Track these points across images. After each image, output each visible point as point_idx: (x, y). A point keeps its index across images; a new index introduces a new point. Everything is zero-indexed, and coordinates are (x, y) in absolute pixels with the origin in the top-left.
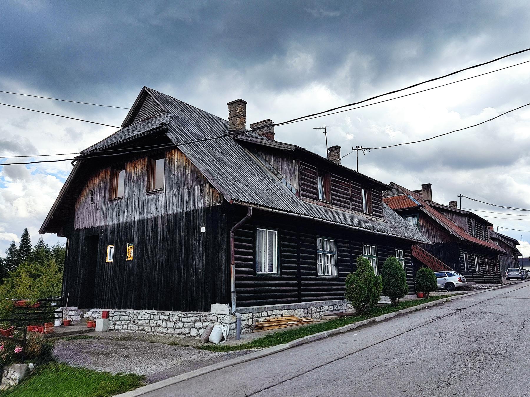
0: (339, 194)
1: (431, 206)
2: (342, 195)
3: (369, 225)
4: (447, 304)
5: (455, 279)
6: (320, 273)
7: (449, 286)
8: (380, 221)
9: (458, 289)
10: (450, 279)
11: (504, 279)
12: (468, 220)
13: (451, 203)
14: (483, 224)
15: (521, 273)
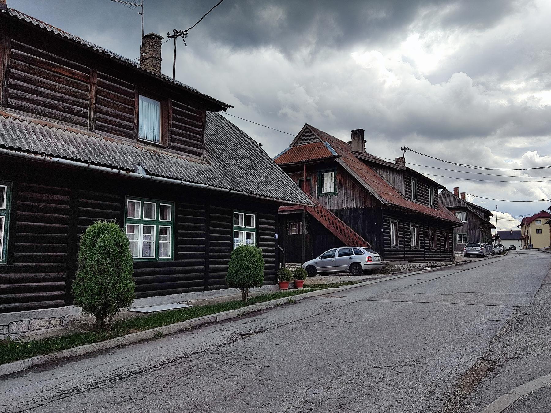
0: (42, 90)
2: (110, 110)
3: (175, 170)
4: (305, 303)
5: (365, 257)
7: (355, 269)
8: (126, 145)
10: (356, 258)
11: (459, 256)
12: (405, 178)
15: (481, 249)
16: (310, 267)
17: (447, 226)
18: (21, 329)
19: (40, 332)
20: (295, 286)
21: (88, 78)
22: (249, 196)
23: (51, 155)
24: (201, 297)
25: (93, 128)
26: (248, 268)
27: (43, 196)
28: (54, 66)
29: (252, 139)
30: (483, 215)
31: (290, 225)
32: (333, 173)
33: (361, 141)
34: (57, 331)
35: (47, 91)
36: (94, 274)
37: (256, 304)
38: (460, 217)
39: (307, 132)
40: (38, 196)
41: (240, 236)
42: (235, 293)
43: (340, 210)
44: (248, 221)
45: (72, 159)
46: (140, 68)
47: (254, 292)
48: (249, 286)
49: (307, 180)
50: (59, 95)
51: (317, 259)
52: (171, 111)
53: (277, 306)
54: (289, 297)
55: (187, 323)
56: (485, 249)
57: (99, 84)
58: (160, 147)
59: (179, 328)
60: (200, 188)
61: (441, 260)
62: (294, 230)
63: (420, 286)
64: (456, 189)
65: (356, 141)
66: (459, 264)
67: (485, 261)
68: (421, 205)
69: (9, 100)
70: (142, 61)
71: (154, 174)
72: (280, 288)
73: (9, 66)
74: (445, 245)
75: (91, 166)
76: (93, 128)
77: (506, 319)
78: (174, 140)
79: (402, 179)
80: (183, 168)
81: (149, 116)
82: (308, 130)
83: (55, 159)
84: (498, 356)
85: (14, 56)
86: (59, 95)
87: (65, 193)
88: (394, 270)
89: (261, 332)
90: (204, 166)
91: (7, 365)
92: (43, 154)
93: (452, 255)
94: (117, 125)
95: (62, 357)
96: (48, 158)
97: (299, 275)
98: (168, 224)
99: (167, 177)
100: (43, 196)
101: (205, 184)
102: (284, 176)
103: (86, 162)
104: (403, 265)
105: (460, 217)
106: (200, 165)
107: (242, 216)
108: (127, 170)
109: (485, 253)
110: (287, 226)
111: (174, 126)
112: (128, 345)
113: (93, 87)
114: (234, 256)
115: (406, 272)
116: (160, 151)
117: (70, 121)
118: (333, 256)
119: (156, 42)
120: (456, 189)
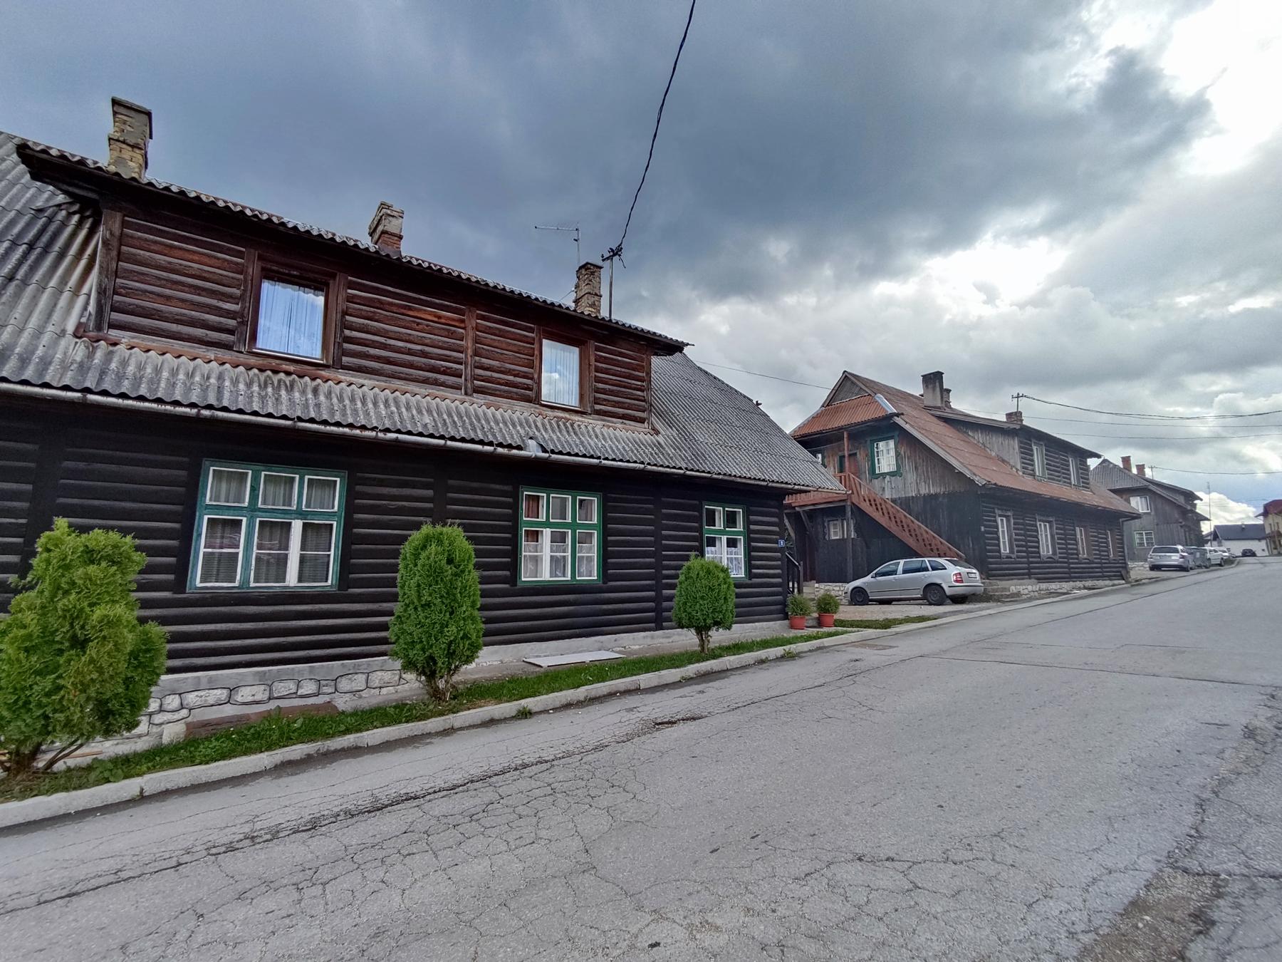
1: (939, 417)
3: (592, 445)
5: (951, 574)
6: (526, 577)
7: (933, 594)
8: (521, 411)
9: (959, 599)
10: (932, 576)
11: (1138, 569)
12: (1021, 442)
13: (1009, 415)
14: (1064, 453)
16: (858, 591)
17: (1111, 520)
18: (355, 686)
19: (384, 691)
20: (820, 623)
21: (463, 321)
23: (387, 430)
24: (649, 641)
25: (469, 391)
26: (702, 598)
27: (394, 491)
30: (1181, 500)
32: (892, 443)
33: (938, 389)
34: (411, 689)
36: (416, 609)
38: (1138, 504)
40: (385, 490)
41: (717, 543)
42: (686, 639)
43: (908, 499)
44: (731, 520)
45: (614, 460)
46: (377, 252)
47: (718, 637)
48: (709, 628)
50: (419, 347)
51: (868, 578)
52: (592, 358)
53: (762, 662)
54: (787, 648)
56: (1190, 558)
57: (477, 328)
58: (576, 412)
59: (564, 701)
60: (634, 470)
61: (1103, 577)
63: (1050, 626)
64: (1126, 460)
65: (930, 390)
66: (1138, 583)
67: (1191, 577)
68: (1055, 485)
69: (345, 359)
70: (576, 301)
71: (553, 452)
72: (792, 627)
73: (345, 313)
74: (1108, 551)
75: (449, 443)
76: (469, 391)
77: (1244, 721)
78: (597, 401)
79: (1015, 443)
80: (613, 441)
81: (560, 371)
82: (847, 380)
83: (393, 436)
84: (1224, 861)
85: (351, 299)
86: (419, 347)
87: (426, 486)
88: (1008, 596)
89: (694, 719)
91: (244, 758)
92: (374, 429)
93: (1125, 567)
95: (339, 747)
96: (381, 435)
98: (738, 533)
99: (577, 455)
100: (394, 491)
102: (803, 453)
103: (442, 437)
104: (1027, 587)
105: (1138, 504)
107: (720, 512)
108: (510, 446)
109: (1191, 564)
111: (598, 380)
112: (461, 729)
114: (682, 578)
115: (1030, 599)
116: (576, 418)
117: (436, 383)
118: (894, 572)
119: (592, 273)
120: (1126, 460)
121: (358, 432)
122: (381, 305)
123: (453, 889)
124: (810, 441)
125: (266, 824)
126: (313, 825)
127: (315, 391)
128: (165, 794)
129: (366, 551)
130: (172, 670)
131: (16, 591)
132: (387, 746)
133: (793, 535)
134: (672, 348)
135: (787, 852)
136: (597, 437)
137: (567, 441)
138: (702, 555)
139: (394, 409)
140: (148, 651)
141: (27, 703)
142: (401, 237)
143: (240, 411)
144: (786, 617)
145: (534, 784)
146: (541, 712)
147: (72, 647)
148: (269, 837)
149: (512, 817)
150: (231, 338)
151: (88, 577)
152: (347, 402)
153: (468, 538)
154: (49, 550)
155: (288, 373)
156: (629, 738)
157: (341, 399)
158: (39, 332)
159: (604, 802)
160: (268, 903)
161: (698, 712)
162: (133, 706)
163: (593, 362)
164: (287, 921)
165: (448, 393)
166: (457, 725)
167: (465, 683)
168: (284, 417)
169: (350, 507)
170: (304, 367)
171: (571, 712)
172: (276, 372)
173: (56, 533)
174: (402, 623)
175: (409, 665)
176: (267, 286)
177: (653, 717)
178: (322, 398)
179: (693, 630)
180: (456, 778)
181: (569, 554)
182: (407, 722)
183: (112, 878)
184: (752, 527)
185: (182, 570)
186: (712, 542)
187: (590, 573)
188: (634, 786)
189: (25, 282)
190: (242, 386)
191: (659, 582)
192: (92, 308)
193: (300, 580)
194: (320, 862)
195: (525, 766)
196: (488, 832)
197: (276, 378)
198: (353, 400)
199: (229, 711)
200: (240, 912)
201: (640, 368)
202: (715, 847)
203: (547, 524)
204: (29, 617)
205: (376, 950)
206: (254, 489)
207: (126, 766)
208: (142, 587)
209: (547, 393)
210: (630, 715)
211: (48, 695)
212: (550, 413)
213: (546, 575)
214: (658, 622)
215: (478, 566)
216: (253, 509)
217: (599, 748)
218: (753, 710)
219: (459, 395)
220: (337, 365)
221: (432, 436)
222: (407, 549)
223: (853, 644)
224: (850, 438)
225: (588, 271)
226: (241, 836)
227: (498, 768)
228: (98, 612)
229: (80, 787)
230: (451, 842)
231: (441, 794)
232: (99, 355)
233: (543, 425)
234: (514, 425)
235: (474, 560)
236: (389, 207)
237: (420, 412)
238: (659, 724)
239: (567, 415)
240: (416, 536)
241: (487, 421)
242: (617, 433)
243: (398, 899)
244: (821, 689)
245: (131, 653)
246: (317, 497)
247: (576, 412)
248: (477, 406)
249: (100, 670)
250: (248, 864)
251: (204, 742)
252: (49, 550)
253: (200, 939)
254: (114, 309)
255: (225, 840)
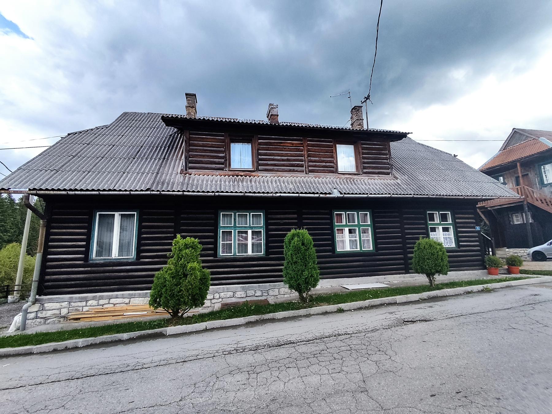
6: (339, 249)
8: (330, 178)
16: (535, 253)
19: (286, 296)
20: (509, 272)
21: (302, 144)
22: (435, 198)
23: (277, 193)
24: (402, 279)
25: (307, 172)
26: (428, 259)
27: (282, 216)
28: (281, 143)
29: (447, 153)
31: (512, 216)
35: (279, 158)
37: (442, 290)
39: (517, 136)
40: (279, 216)
42: (421, 279)
44: (444, 218)
47: (439, 278)
48: (434, 274)
49: (523, 176)
50: (286, 158)
51: (545, 246)
52: (360, 149)
53: (469, 293)
54: (485, 286)
55: (367, 303)
58: (355, 174)
62: (518, 221)
70: (352, 125)
71: (345, 193)
72: (490, 273)
73: (258, 150)
75: (300, 195)
78: (365, 168)
80: (375, 186)
86: (286, 158)
89: (426, 321)
90: (392, 181)
91: (236, 319)
94: (322, 167)
96: (274, 195)
97: (512, 261)
98: (368, 225)
99: (356, 194)
101: (390, 194)
103: (297, 193)
106: (389, 181)
110: (509, 217)
111: (364, 158)
112: (314, 315)
113: (306, 148)
114: (416, 249)
117: (294, 171)
119: (358, 110)
121: (266, 194)
122: (270, 144)
123: (304, 387)
124: (492, 172)
125: (241, 345)
126: (256, 349)
127: (251, 181)
128: (213, 329)
129: (274, 242)
130: (212, 285)
131: (169, 258)
132: (285, 319)
133: (487, 222)
134: (400, 136)
135: (479, 406)
136: (366, 184)
137: (351, 188)
138: (428, 236)
139: (279, 184)
140: (205, 279)
141: (174, 295)
142: (278, 115)
143: (227, 192)
144: (485, 268)
145: (342, 344)
146: (348, 311)
147: (183, 277)
148: (242, 351)
149: (331, 358)
150: (223, 166)
151: (186, 253)
152: (262, 184)
153: (310, 234)
154: (176, 245)
155: (242, 176)
156: (389, 327)
157: (259, 183)
158: (172, 174)
159: (375, 358)
160: (238, 377)
161: (428, 318)
162: (202, 298)
163: (361, 151)
164: (243, 386)
165: (299, 174)
166: (312, 313)
167: (315, 295)
168: (241, 192)
169: (267, 224)
170: (247, 173)
171: (362, 312)
172: (237, 176)
173: (177, 239)
174: (287, 270)
175: (291, 287)
176: (232, 145)
177: (402, 318)
178: (253, 183)
179: (425, 275)
180: (310, 337)
181: (358, 239)
182: (292, 310)
183: (195, 358)
184: (457, 220)
185: (215, 249)
186: (433, 230)
187: (369, 247)
188: (390, 352)
189: (168, 159)
190: (227, 183)
191: (405, 251)
192: (184, 164)
193: (253, 252)
194: (257, 364)
195: (339, 335)
196: (320, 363)
197: (237, 178)
198: (264, 182)
199: (234, 300)
200: (229, 379)
201: (385, 149)
202: (433, 393)
203: (346, 226)
204: (172, 267)
205: (272, 407)
206: (235, 219)
207: (202, 318)
208: (202, 256)
209: (341, 169)
210: (391, 316)
211: (179, 292)
212: (343, 176)
213: (348, 248)
214: (407, 270)
215: (315, 246)
216: (235, 226)
217: (374, 330)
218: (462, 319)
219: (303, 174)
220: (258, 170)
221: (293, 193)
222: (286, 239)
223: (533, 285)
224: (522, 165)
225: (356, 110)
226: (233, 349)
227: (327, 334)
228: (189, 265)
229: (190, 324)
230: (305, 365)
231: (303, 343)
232: (187, 178)
233: (340, 182)
234: (327, 184)
235: (313, 243)
236: (272, 105)
237: (288, 184)
238: (406, 322)
239: (350, 176)
240: (290, 234)
241: (315, 184)
242: (376, 181)
243: (283, 386)
244: (509, 311)
245: (200, 279)
246: (255, 221)
247: (355, 174)
248: (311, 178)
249: (192, 285)
250: (233, 360)
251: (230, 311)
252: (176, 245)
253: (216, 386)
254: (189, 163)
255: (229, 349)
